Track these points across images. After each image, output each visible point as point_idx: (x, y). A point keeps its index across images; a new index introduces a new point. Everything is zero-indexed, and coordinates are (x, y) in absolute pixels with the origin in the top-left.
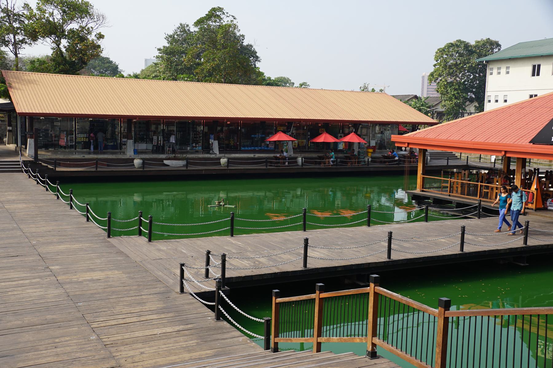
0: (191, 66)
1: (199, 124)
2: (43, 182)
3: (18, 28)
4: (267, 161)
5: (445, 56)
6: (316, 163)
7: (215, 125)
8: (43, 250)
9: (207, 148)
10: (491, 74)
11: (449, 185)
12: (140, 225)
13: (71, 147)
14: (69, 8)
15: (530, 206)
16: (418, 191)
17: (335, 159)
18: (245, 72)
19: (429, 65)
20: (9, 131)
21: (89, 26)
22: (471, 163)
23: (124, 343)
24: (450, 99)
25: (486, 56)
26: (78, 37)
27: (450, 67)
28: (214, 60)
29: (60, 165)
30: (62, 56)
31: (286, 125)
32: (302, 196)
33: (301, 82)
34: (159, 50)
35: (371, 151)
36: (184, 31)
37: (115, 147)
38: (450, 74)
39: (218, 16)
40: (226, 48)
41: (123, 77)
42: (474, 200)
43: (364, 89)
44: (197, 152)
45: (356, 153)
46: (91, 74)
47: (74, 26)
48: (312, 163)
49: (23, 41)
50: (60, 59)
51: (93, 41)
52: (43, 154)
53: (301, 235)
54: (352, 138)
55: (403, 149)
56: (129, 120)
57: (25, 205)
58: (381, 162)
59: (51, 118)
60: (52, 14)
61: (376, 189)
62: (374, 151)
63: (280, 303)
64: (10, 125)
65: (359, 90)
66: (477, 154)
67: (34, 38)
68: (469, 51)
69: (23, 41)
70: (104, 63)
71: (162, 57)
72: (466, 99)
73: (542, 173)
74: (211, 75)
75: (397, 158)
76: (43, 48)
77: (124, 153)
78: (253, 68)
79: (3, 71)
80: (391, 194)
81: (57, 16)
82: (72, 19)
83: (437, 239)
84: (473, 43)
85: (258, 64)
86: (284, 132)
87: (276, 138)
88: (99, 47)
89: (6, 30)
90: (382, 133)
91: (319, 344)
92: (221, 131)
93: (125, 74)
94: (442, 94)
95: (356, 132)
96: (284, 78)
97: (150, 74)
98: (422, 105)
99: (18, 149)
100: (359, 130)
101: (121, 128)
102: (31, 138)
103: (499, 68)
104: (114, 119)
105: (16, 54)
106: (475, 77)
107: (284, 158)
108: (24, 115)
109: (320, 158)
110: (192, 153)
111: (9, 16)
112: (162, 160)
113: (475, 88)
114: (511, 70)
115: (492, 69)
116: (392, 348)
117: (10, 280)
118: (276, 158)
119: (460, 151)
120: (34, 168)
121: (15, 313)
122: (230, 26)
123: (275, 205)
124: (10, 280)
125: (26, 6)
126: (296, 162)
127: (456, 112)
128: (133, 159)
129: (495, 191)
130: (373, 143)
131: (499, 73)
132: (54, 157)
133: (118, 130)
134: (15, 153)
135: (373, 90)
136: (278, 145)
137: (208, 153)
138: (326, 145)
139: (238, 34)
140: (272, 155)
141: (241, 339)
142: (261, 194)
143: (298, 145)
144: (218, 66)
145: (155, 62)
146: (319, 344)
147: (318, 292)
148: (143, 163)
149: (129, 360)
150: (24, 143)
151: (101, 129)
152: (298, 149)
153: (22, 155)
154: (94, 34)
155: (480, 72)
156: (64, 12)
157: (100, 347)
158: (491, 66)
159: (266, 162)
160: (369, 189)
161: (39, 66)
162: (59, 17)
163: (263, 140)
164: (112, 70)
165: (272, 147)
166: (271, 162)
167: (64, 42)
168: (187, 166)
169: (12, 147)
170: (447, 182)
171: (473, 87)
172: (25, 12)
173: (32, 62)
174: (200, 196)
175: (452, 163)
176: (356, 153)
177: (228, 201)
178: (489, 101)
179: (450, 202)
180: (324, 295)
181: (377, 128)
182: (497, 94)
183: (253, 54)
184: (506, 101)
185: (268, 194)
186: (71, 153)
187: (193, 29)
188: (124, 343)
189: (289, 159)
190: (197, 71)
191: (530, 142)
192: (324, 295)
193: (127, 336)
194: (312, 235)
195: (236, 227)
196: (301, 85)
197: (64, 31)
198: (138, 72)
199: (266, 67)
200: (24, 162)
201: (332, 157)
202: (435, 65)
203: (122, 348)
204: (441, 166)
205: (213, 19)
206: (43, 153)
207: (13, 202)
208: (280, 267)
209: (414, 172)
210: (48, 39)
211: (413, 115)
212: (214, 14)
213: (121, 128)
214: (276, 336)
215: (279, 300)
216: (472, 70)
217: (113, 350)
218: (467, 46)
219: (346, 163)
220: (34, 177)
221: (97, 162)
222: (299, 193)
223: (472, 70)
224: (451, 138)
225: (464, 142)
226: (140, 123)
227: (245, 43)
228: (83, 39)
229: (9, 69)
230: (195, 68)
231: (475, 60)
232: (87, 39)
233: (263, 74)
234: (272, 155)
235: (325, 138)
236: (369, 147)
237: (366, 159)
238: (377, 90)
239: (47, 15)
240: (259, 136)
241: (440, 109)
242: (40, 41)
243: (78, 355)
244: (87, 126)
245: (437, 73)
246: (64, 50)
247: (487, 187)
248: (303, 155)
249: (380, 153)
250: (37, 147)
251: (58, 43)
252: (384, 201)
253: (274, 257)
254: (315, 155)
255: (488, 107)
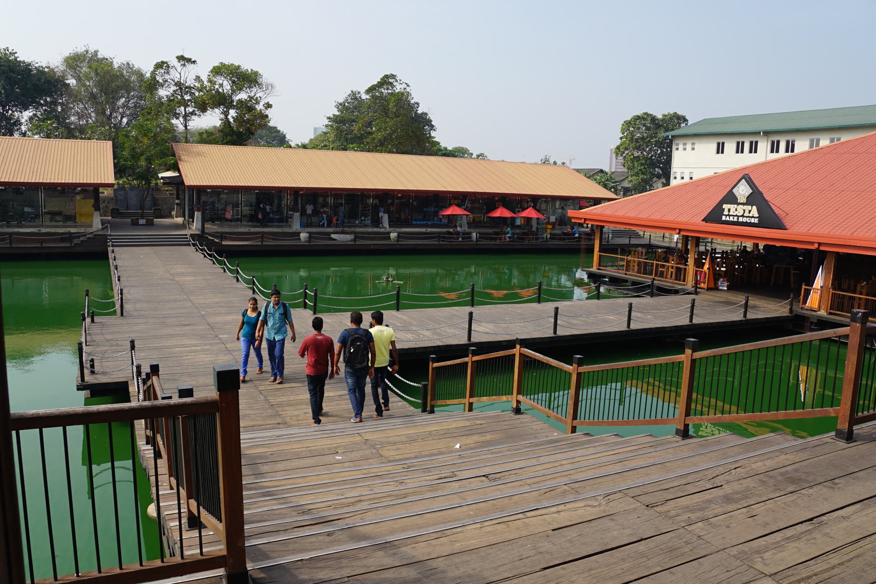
0: (362, 135)
1: (369, 197)
2: (210, 255)
3: (189, 100)
4: (439, 236)
5: (631, 129)
6: (491, 239)
7: (385, 197)
8: (212, 320)
9: (377, 222)
10: (677, 149)
11: (625, 263)
12: (306, 298)
13: (237, 220)
14: (239, 79)
15: (702, 285)
16: (594, 269)
17: (513, 234)
18: (418, 142)
19: (615, 138)
20: (177, 204)
21: (258, 95)
22: (653, 242)
23: (290, 404)
24: (637, 174)
25: (673, 130)
26: (246, 107)
27: (637, 140)
28: (385, 129)
29: (226, 239)
30: (230, 126)
31: (460, 198)
32: (475, 274)
33: (478, 153)
34: (328, 118)
35: (550, 227)
36: (356, 99)
37: (281, 220)
38: (638, 148)
39: (391, 84)
40: (398, 117)
41: (290, 147)
42: (647, 279)
43: (546, 162)
44: (366, 226)
45: (534, 229)
46: (257, 144)
47: (243, 96)
48: (487, 239)
49: (193, 113)
50: (227, 130)
51: (261, 110)
52: (210, 227)
53: (468, 309)
54: (530, 213)
55: (585, 225)
56: (295, 192)
57: (193, 278)
58: (560, 239)
59: (217, 191)
60: (221, 85)
61: (554, 268)
62: (554, 228)
63: (436, 368)
64: (178, 198)
65: (539, 162)
66: (660, 233)
67: (203, 109)
68: (656, 124)
69: (193, 113)
70: (272, 133)
71: (331, 126)
72: (653, 175)
73: (718, 253)
74: (382, 145)
75: (577, 235)
76: (212, 119)
77: (290, 226)
78: (428, 138)
79: (174, 144)
80: (570, 274)
81: (227, 86)
82: (241, 89)
83: (606, 316)
84: (660, 116)
85: (433, 134)
86: (458, 205)
87: (449, 212)
88: (267, 116)
89: (178, 103)
90: (562, 208)
91: (471, 404)
92: (392, 204)
93: (293, 144)
94: (628, 169)
95: (534, 207)
96: (463, 148)
97: (319, 144)
98: (608, 180)
99: (186, 222)
100: (538, 205)
101: (287, 200)
102: (198, 211)
103: (685, 144)
104: (280, 191)
105: (186, 126)
106: (662, 151)
107: (458, 233)
108: (192, 188)
109: (496, 233)
110: (361, 227)
111: (181, 89)
112: (329, 234)
113: (663, 163)
114: (696, 146)
115: (677, 145)
116: (539, 406)
117: (184, 346)
118: (449, 233)
119: (644, 229)
120: (201, 240)
121: (190, 375)
122: (403, 94)
123: (448, 284)
124: (184, 346)
125: (198, 78)
126: (471, 237)
127: (643, 187)
128: (299, 233)
129: (670, 270)
130: (553, 219)
131: (685, 149)
132: (220, 230)
133: (284, 202)
134: (183, 227)
135: (555, 163)
136: (452, 219)
137: (378, 227)
138: (503, 220)
139: (412, 102)
140: (445, 230)
141: (400, 404)
142: (434, 271)
143: (474, 219)
144: (390, 135)
145: (325, 131)
146: (471, 404)
147: (470, 355)
148: (310, 237)
149: (294, 418)
150: (192, 216)
151: (267, 202)
152: (473, 224)
153: (190, 228)
154: (262, 103)
155: (668, 146)
156: (234, 82)
157: (267, 406)
158: (677, 142)
159: (439, 237)
160: (547, 268)
161: (207, 137)
162: (229, 87)
163: (436, 213)
164: (279, 140)
165: (445, 221)
166: (444, 238)
167: (232, 113)
168: (355, 240)
169: (180, 220)
170: (623, 260)
171: (660, 162)
172: (196, 84)
173: (201, 134)
174: (368, 273)
175: (634, 241)
176: (534, 229)
177: (398, 277)
178: (675, 178)
179: (626, 281)
180: (476, 358)
181: (558, 203)
182: (683, 170)
183: (429, 122)
184: (682, 178)
185: (440, 271)
186: (237, 226)
187: (364, 97)
188: (290, 404)
189: (463, 234)
190: (368, 140)
191: (703, 220)
192: (476, 358)
193: (292, 398)
194: (477, 310)
195: (401, 302)
196: (478, 156)
197: (232, 101)
198: (306, 141)
199: (443, 136)
200: (191, 235)
201: (508, 233)
202: (621, 138)
203: (287, 408)
204: (621, 245)
205: (385, 86)
206: (210, 226)
207: (182, 274)
208: (444, 340)
209: (591, 251)
210: (216, 110)
211: (600, 192)
212: (387, 81)
213: (287, 200)
214: (433, 399)
215: (436, 365)
216: (659, 144)
217: (278, 409)
218: (653, 119)
219: (524, 239)
220: (202, 250)
221: (263, 236)
222: (473, 270)
223: (659, 144)
224: (628, 215)
225: (667, 222)
226: (307, 195)
227: (420, 112)
228: (251, 109)
229: (177, 142)
230: (366, 138)
231: (662, 134)
232: (255, 109)
233: (438, 143)
234: (445, 230)
235: (501, 212)
236: (548, 223)
237: (545, 236)
238: (559, 163)
239: (217, 87)
240: (432, 209)
241: (626, 184)
242: (209, 112)
243: (247, 412)
244: (253, 199)
245: (624, 146)
246: (231, 120)
247: (663, 266)
248: (478, 230)
249: (560, 229)
250: (204, 221)
251: (226, 114)
252: (564, 279)
253: (438, 331)
254: (490, 231)
255: (673, 183)
